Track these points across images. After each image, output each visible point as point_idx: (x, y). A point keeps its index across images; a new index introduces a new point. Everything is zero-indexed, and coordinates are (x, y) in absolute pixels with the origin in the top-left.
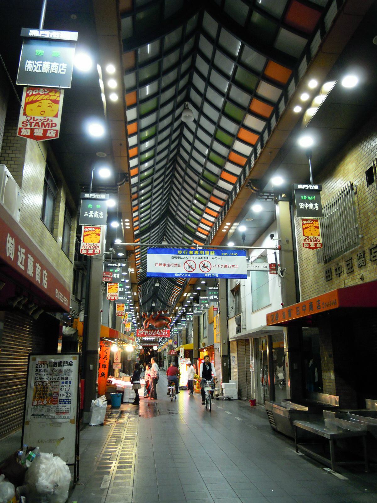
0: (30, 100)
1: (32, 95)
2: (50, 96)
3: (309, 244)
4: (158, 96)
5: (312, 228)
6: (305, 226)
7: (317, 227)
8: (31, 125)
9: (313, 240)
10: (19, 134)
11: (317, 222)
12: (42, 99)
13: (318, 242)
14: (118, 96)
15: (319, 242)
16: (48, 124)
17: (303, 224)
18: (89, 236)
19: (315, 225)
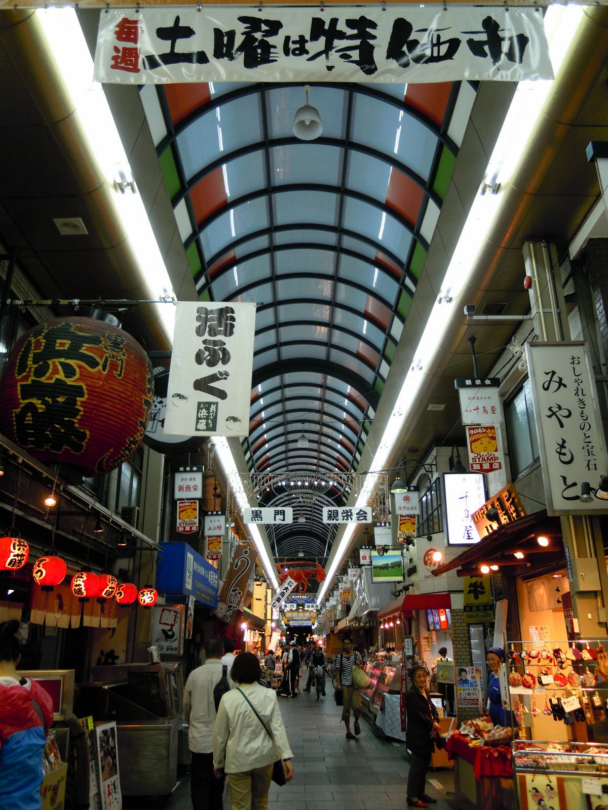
1: (474, 434)
3: (481, 465)
7: (414, 524)
10: (472, 469)
14: (514, 404)
15: (497, 461)
16: (492, 458)
19: (412, 521)
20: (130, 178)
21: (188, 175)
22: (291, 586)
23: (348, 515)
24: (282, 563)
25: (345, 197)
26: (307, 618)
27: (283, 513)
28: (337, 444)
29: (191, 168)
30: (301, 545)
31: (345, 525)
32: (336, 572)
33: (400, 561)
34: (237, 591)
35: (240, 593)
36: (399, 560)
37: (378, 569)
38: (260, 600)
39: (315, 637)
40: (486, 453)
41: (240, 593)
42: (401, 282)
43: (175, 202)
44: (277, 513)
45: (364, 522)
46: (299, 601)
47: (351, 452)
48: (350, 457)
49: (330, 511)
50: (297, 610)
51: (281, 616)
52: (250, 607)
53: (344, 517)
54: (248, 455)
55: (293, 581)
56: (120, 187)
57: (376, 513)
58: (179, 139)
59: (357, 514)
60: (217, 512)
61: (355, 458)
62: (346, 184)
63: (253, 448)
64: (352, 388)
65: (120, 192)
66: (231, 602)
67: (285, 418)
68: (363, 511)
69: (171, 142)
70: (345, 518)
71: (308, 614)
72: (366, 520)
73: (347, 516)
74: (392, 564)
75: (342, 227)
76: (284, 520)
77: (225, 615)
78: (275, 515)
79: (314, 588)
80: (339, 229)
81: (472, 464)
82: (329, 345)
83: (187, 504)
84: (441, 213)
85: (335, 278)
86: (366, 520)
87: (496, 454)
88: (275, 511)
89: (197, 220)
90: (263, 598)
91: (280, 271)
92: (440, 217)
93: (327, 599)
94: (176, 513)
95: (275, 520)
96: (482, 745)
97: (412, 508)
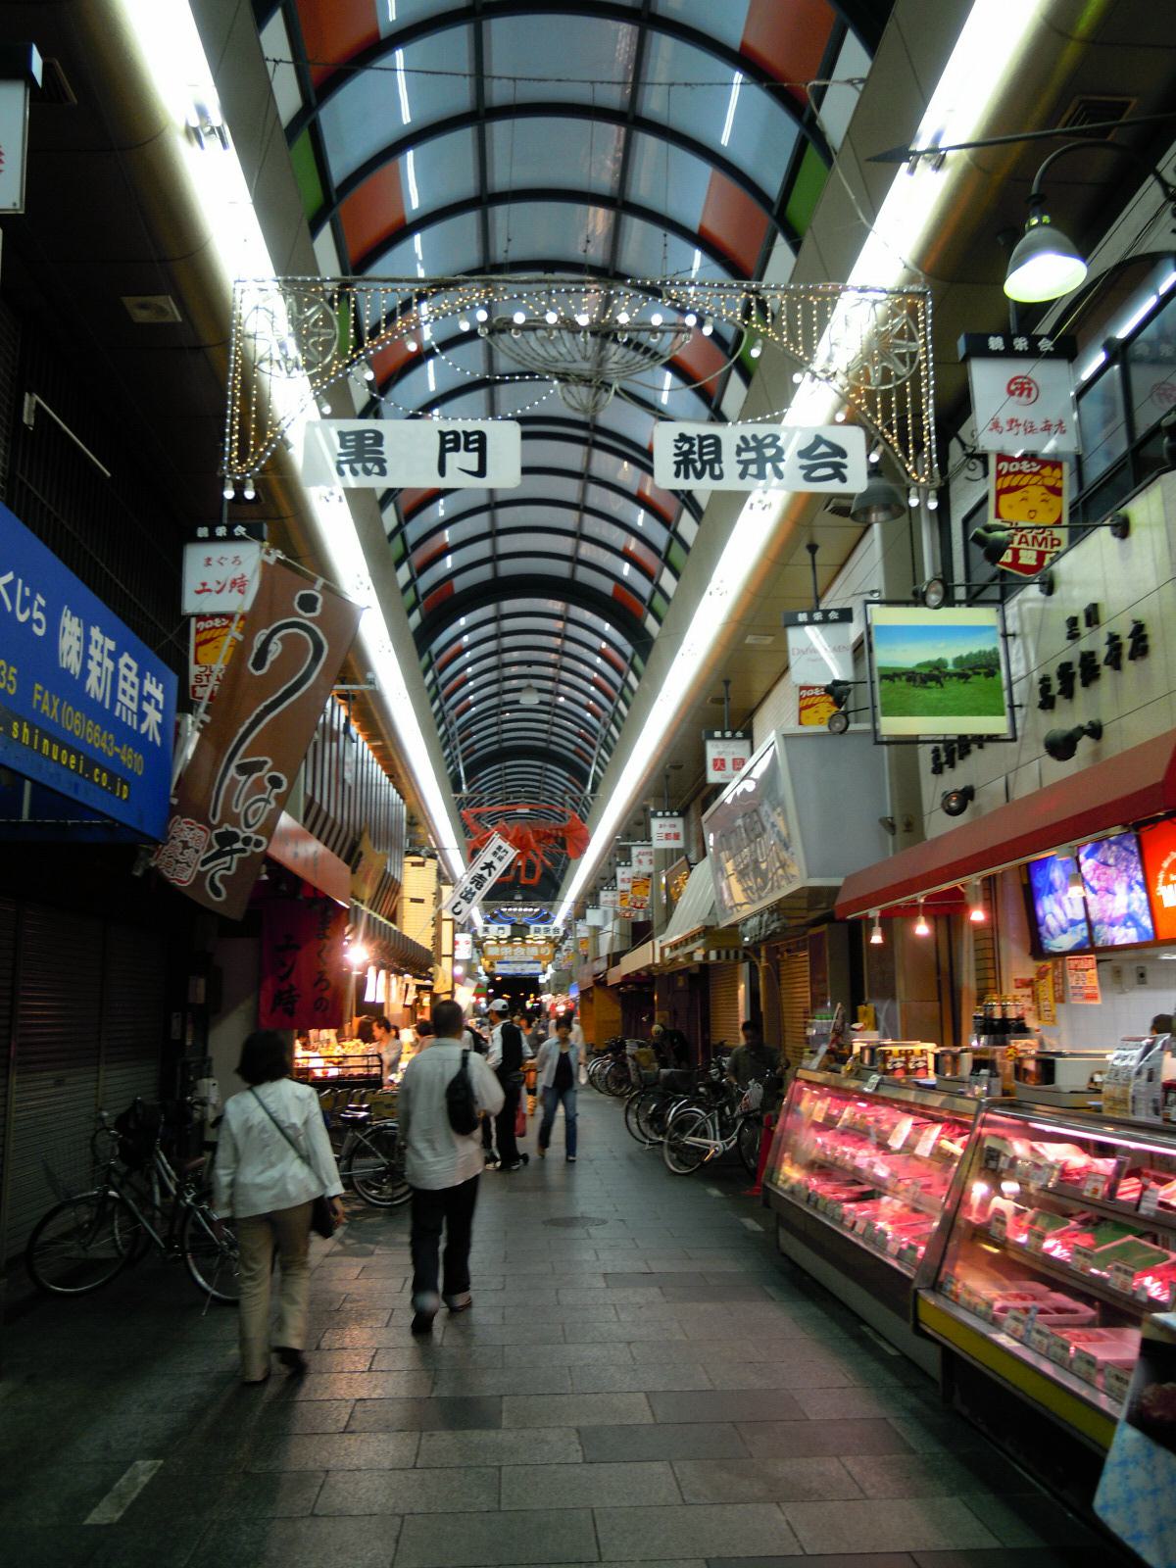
0: (1005, 485)
2: (1043, 477)
4: (1134, 445)
6: (1006, 482)
7: (1056, 491)
9: (1034, 538)
11: (1057, 472)
13: (1052, 546)
17: (999, 474)
18: (813, 709)
19: (1050, 482)
20: (217, 118)
21: (338, 171)
22: (500, 859)
23: (760, 456)
24: (475, 810)
25: (649, 32)
26: (531, 959)
27: (478, 443)
28: (619, 560)
29: (341, 165)
30: (523, 786)
31: (739, 499)
32: (615, 832)
33: (995, 652)
34: (265, 774)
35: (275, 782)
36: (988, 648)
37: (901, 683)
38: (421, 901)
39: (546, 998)
41: (275, 782)
42: (713, 406)
43: (314, 228)
44: (450, 442)
45: (834, 486)
46: (517, 920)
47: (649, 575)
48: (618, 681)
49: (683, 438)
50: (510, 939)
51: (476, 956)
52: (393, 918)
53: (746, 463)
54: (430, 676)
55: (506, 846)
56: (193, 134)
57: (884, 456)
58: (325, 115)
59: (802, 454)
60: (230, 529)
61: (626, 682)
62: (627, 191)
63: (418, 557)
64: (709, 261)
65: (196, 144)
66: (230, 817)
67: (494, 546)
68: (829, 444)
69: (308, 122)
70: (753, 469)
71: (534, 951)
72: (843, 479)
73: (761, 461)
74: (958, 661)
75: (626, 198)
76: (481, 472)
77: (201, 876)
78: (443, 451)
79: (548, 888)
80: (630, 117)
81: (194, 687)
82: (575, 560)
84: (747, 396)
85: (620, 204)
86: (843, 479)
88: (443, 434)
89: (314, 73)
90: (429, 899)
91: (502, 178)
92: (857, 106)
93: (579, 913)
95: (442, 471)
96: (893, 1248)
97: (1047, 427)
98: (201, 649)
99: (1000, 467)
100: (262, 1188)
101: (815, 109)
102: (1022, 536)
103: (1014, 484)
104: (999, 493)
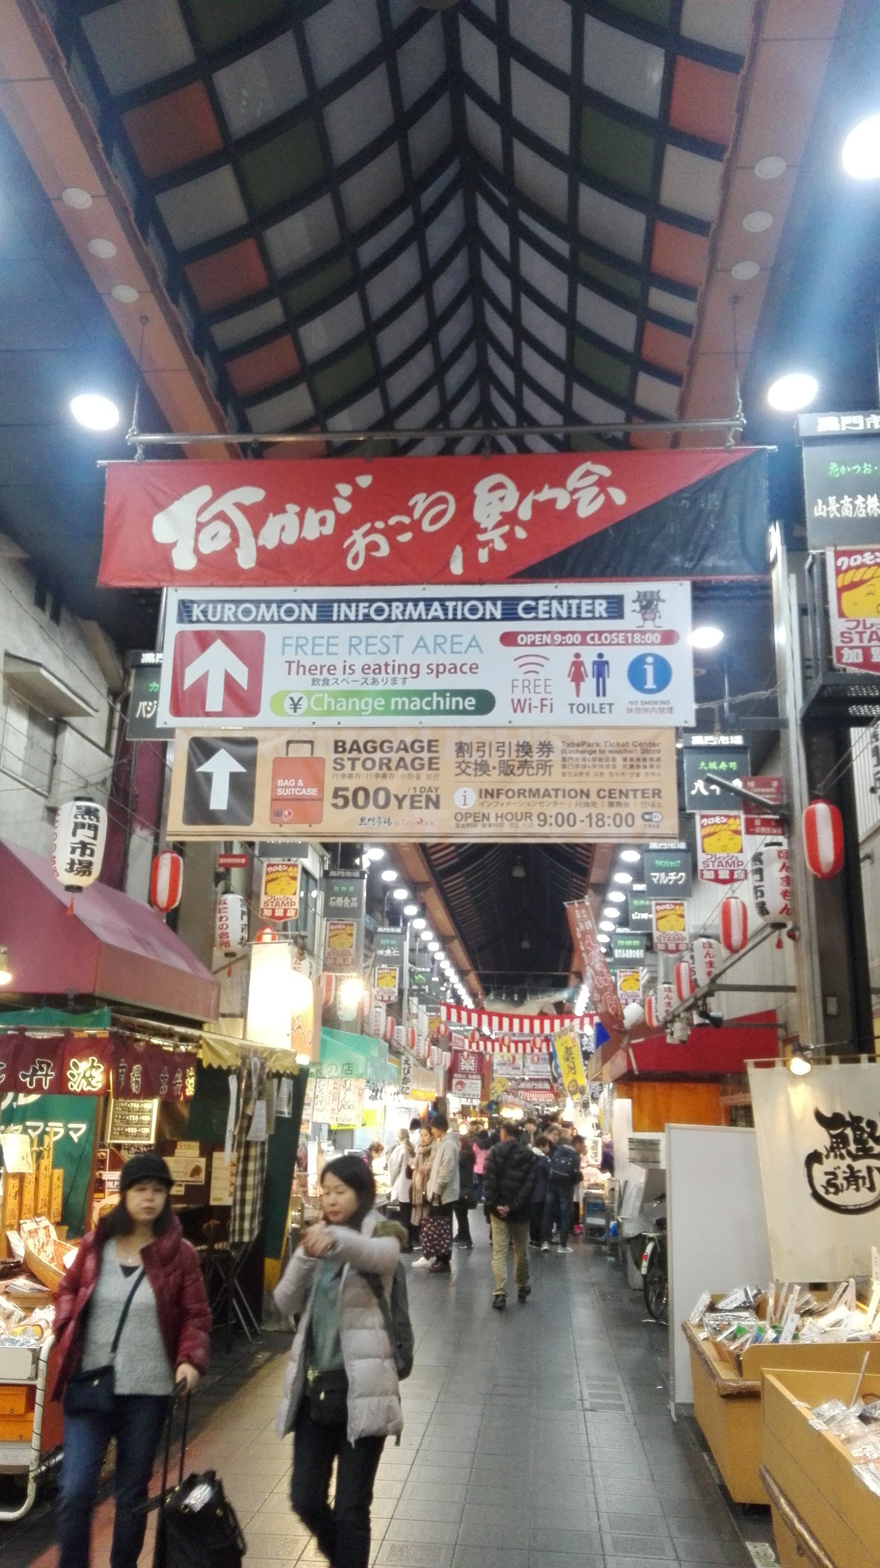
0: (847, 582)
3: (716, 872)
5: (725, 836)
6: (848, 579)
8: (861, 641)
11: (738, 821)
12: (873, 578)
13: (739, 865)
15: (741, 867)
17: (657, 911)
19: (679, 912)
40: (725, 855)
81: (702, 871)
83: (668, 907)
87: (741, 857)
94: (261, 884)
98: (270, 885)
99: (839, 563)
100: (444, 1187)
101: (586, 428)
102: (872, 633)
103: (856, 579)
104: (658, 919)
